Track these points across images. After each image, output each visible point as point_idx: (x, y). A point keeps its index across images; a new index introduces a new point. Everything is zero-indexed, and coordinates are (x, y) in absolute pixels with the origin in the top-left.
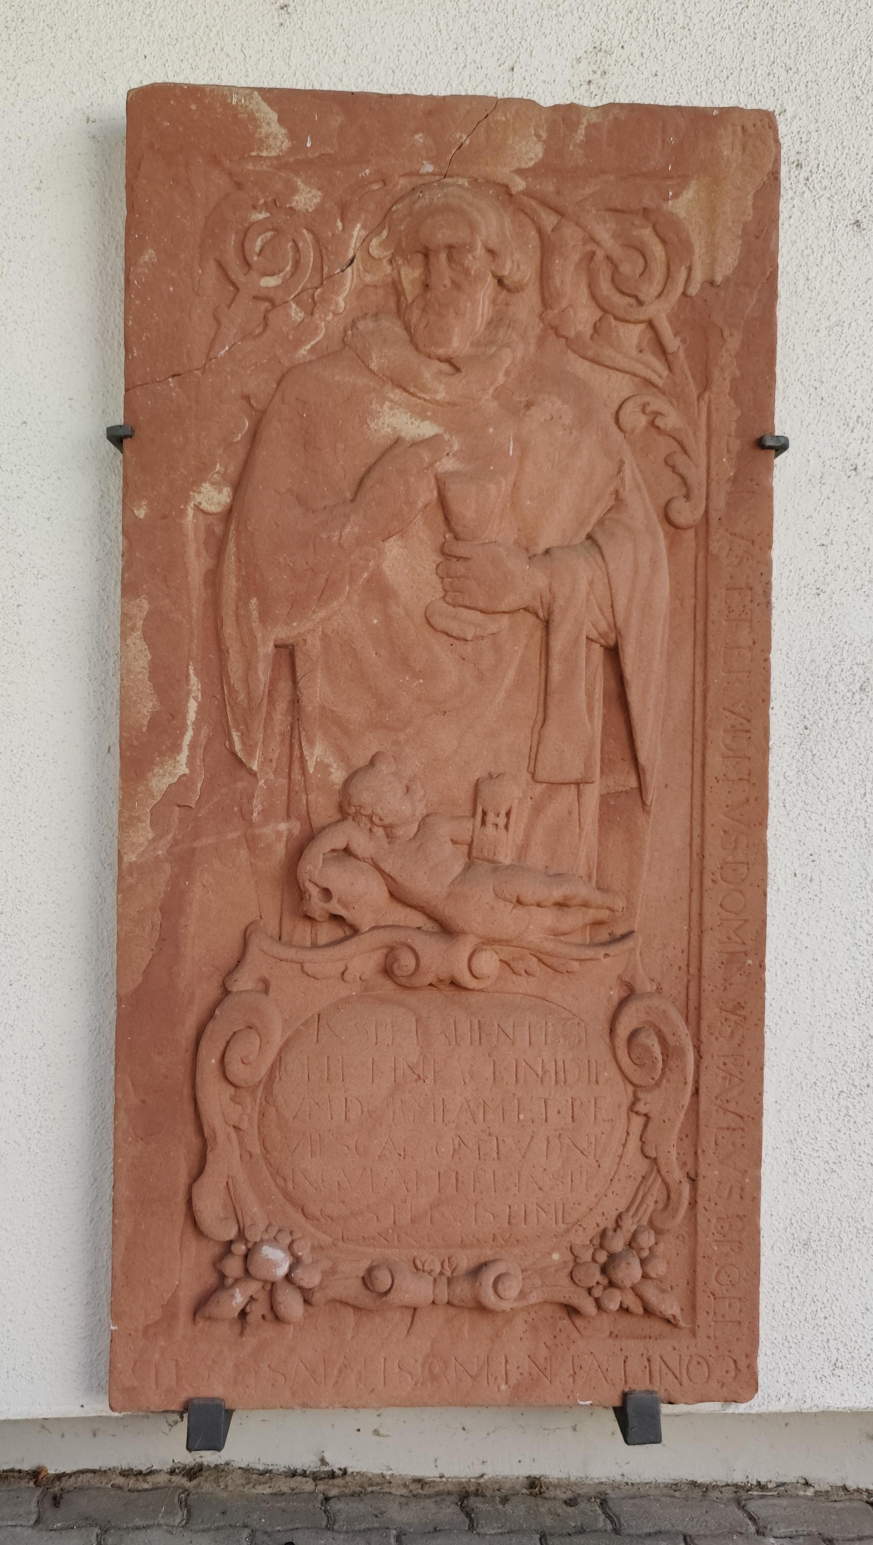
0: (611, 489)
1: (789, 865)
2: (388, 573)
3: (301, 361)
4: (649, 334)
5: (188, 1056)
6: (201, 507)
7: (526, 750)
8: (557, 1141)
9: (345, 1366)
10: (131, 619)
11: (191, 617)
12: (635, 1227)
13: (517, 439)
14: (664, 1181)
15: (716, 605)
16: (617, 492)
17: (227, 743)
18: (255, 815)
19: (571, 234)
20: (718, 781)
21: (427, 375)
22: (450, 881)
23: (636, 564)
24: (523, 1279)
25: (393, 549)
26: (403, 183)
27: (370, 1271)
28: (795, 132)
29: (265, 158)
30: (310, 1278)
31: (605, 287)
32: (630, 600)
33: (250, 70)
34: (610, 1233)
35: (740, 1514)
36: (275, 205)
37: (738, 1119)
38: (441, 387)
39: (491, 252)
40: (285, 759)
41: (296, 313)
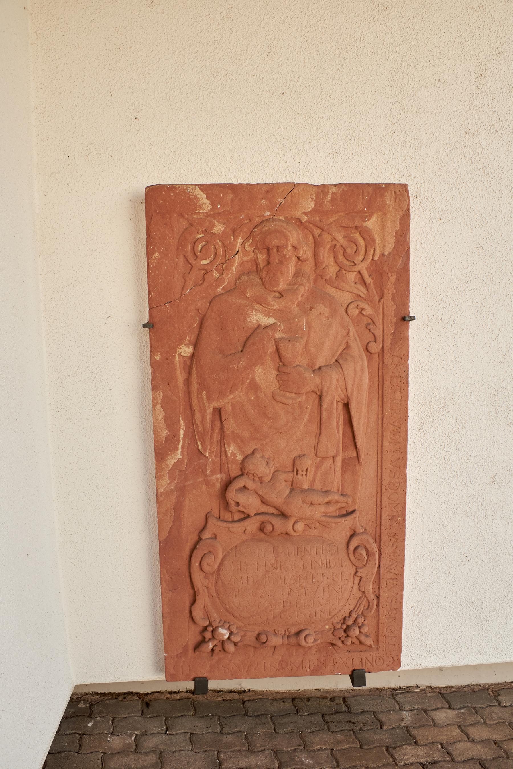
0: (345, 341)
1: (415, 476)
2: (257, 379)
3: (219, 293)
4: (359, 276)
5: (187, 562)
6: (181, 354)
7: (313, 445)
8: (327, 588)
9: (250, 666)
10: (156, 400)
11: (179, 398)
12: (356, 616)
13: (307, 323)
14: (367, 599)
15: (387, 384)
16: (347, 342)
17: (196, 445)
18: (208, 472)
19: (326, 237)
20: (388, 452)
21: (270, 299)
22: (285, 497)
23: (355, 371)
24: (315, 635)
25: (259, 370)
26: (257, 220)
27: (259, 635)
28: (415, 184)
29: (201, 213)
30: (236, 638)
31: (341, 258)
32: (353, 385)
33: (192, 168)
34: (347, 618)
35: (393, 701)
36: (205, 232)
37: (395, 575)
38: (276, 304)
39: (294, 247)
40: (219, 451)
41: (216, 274)
